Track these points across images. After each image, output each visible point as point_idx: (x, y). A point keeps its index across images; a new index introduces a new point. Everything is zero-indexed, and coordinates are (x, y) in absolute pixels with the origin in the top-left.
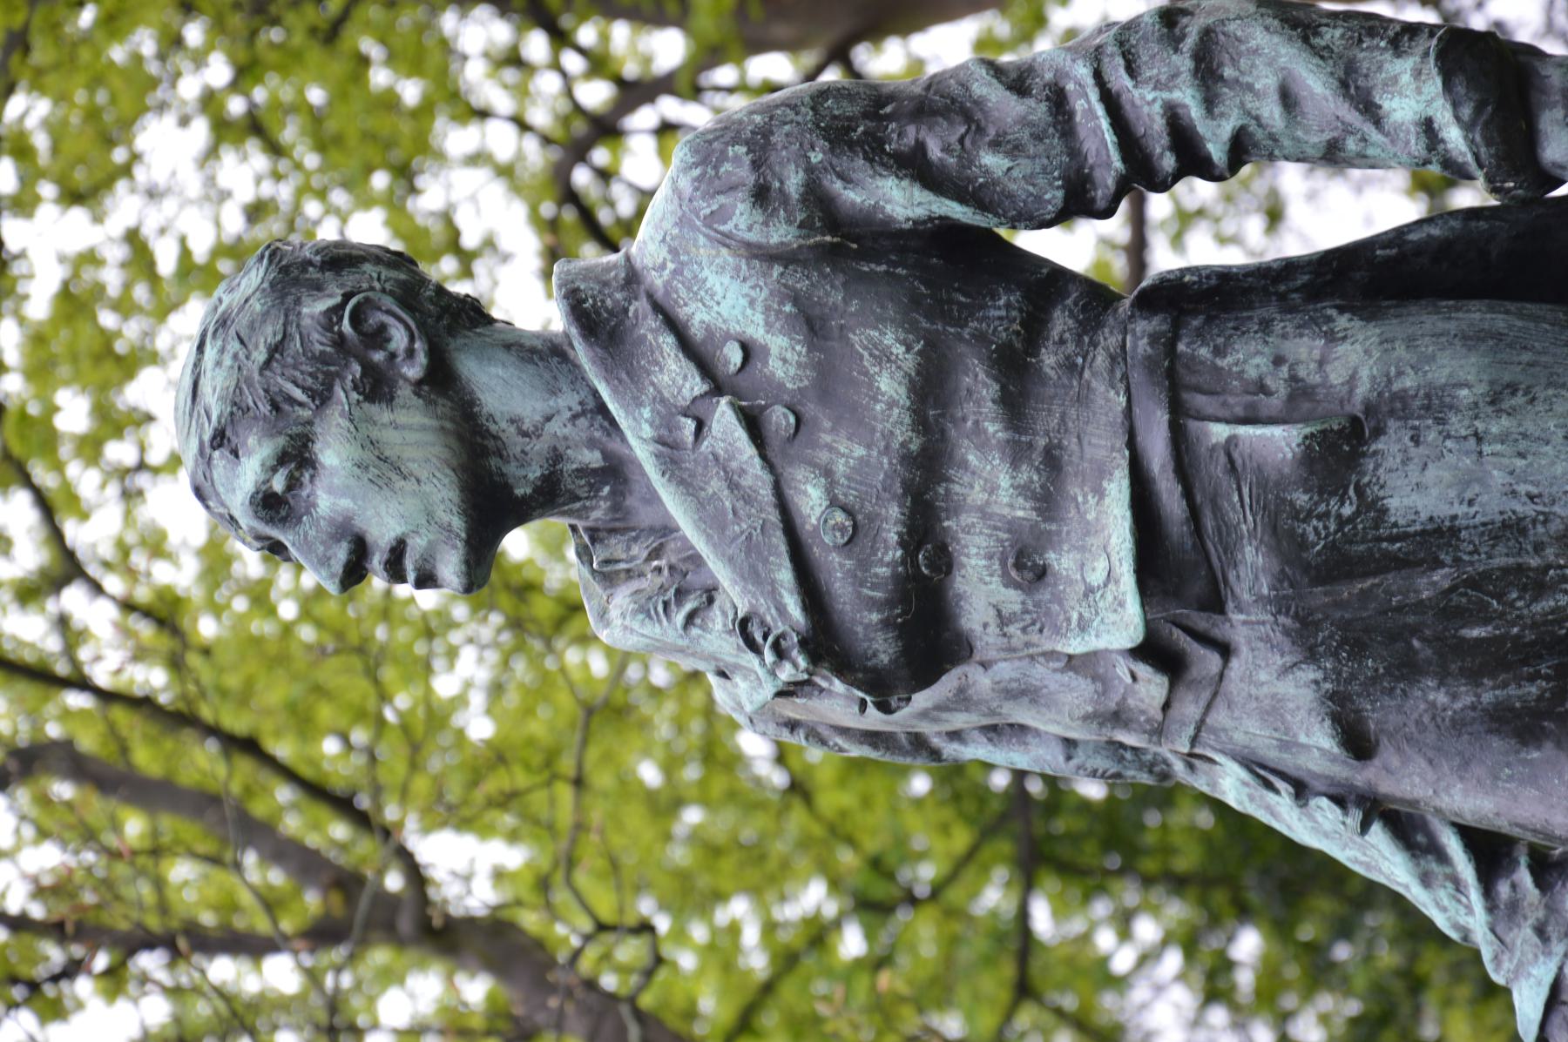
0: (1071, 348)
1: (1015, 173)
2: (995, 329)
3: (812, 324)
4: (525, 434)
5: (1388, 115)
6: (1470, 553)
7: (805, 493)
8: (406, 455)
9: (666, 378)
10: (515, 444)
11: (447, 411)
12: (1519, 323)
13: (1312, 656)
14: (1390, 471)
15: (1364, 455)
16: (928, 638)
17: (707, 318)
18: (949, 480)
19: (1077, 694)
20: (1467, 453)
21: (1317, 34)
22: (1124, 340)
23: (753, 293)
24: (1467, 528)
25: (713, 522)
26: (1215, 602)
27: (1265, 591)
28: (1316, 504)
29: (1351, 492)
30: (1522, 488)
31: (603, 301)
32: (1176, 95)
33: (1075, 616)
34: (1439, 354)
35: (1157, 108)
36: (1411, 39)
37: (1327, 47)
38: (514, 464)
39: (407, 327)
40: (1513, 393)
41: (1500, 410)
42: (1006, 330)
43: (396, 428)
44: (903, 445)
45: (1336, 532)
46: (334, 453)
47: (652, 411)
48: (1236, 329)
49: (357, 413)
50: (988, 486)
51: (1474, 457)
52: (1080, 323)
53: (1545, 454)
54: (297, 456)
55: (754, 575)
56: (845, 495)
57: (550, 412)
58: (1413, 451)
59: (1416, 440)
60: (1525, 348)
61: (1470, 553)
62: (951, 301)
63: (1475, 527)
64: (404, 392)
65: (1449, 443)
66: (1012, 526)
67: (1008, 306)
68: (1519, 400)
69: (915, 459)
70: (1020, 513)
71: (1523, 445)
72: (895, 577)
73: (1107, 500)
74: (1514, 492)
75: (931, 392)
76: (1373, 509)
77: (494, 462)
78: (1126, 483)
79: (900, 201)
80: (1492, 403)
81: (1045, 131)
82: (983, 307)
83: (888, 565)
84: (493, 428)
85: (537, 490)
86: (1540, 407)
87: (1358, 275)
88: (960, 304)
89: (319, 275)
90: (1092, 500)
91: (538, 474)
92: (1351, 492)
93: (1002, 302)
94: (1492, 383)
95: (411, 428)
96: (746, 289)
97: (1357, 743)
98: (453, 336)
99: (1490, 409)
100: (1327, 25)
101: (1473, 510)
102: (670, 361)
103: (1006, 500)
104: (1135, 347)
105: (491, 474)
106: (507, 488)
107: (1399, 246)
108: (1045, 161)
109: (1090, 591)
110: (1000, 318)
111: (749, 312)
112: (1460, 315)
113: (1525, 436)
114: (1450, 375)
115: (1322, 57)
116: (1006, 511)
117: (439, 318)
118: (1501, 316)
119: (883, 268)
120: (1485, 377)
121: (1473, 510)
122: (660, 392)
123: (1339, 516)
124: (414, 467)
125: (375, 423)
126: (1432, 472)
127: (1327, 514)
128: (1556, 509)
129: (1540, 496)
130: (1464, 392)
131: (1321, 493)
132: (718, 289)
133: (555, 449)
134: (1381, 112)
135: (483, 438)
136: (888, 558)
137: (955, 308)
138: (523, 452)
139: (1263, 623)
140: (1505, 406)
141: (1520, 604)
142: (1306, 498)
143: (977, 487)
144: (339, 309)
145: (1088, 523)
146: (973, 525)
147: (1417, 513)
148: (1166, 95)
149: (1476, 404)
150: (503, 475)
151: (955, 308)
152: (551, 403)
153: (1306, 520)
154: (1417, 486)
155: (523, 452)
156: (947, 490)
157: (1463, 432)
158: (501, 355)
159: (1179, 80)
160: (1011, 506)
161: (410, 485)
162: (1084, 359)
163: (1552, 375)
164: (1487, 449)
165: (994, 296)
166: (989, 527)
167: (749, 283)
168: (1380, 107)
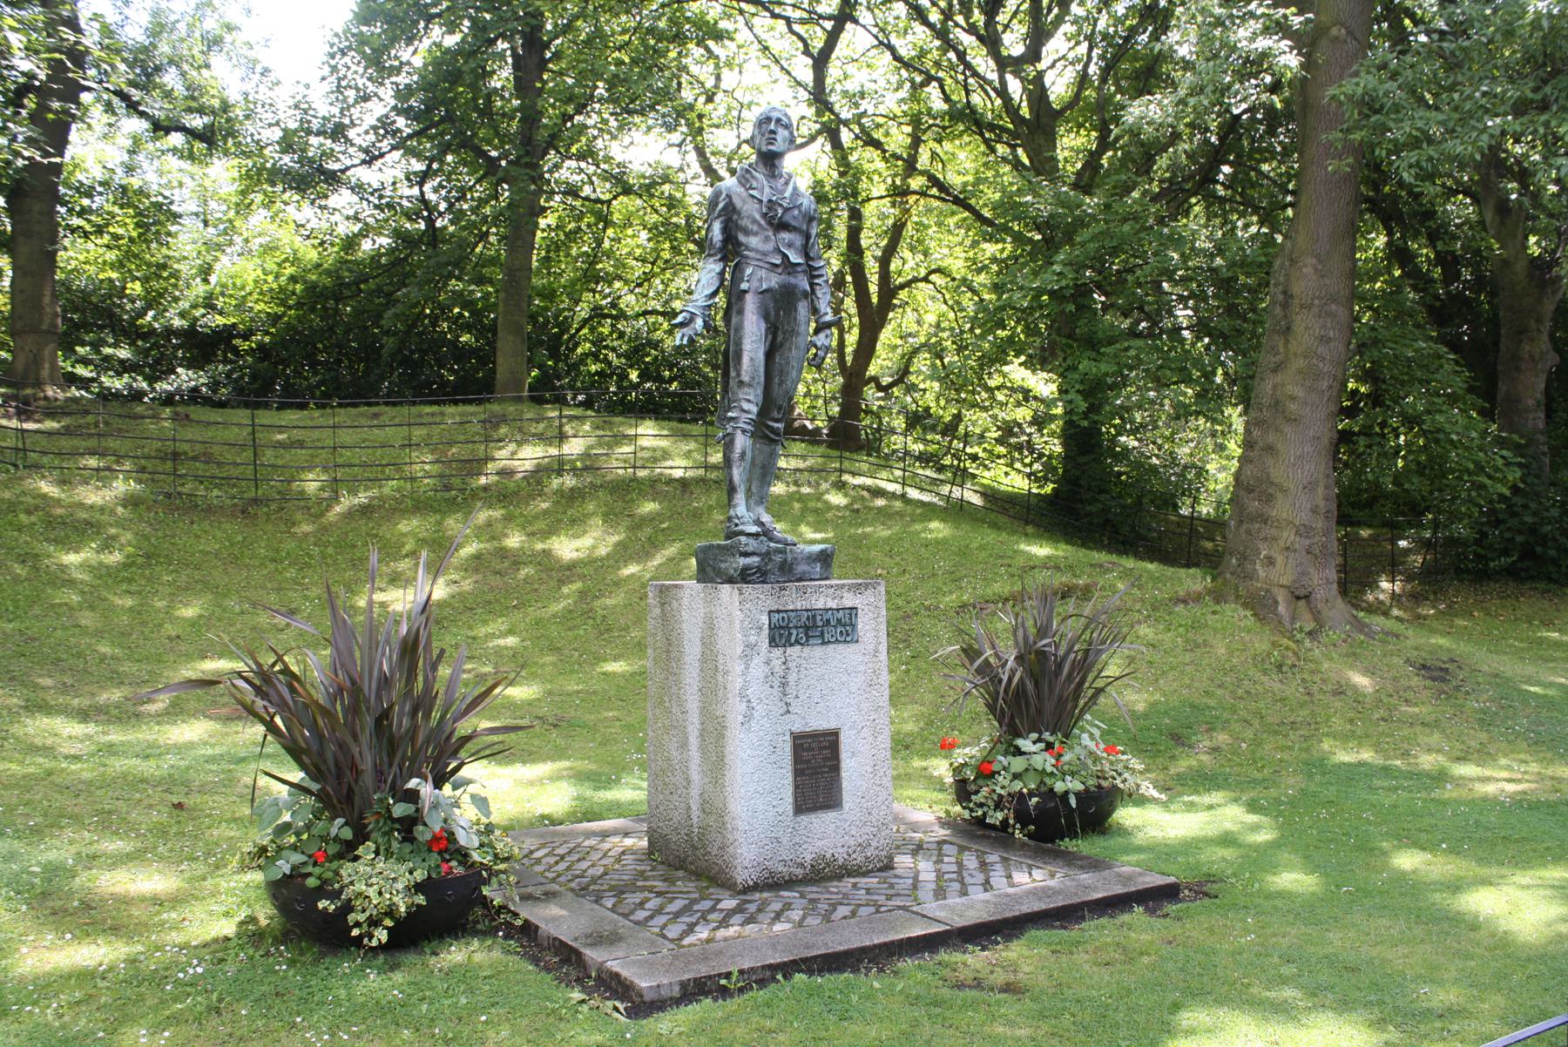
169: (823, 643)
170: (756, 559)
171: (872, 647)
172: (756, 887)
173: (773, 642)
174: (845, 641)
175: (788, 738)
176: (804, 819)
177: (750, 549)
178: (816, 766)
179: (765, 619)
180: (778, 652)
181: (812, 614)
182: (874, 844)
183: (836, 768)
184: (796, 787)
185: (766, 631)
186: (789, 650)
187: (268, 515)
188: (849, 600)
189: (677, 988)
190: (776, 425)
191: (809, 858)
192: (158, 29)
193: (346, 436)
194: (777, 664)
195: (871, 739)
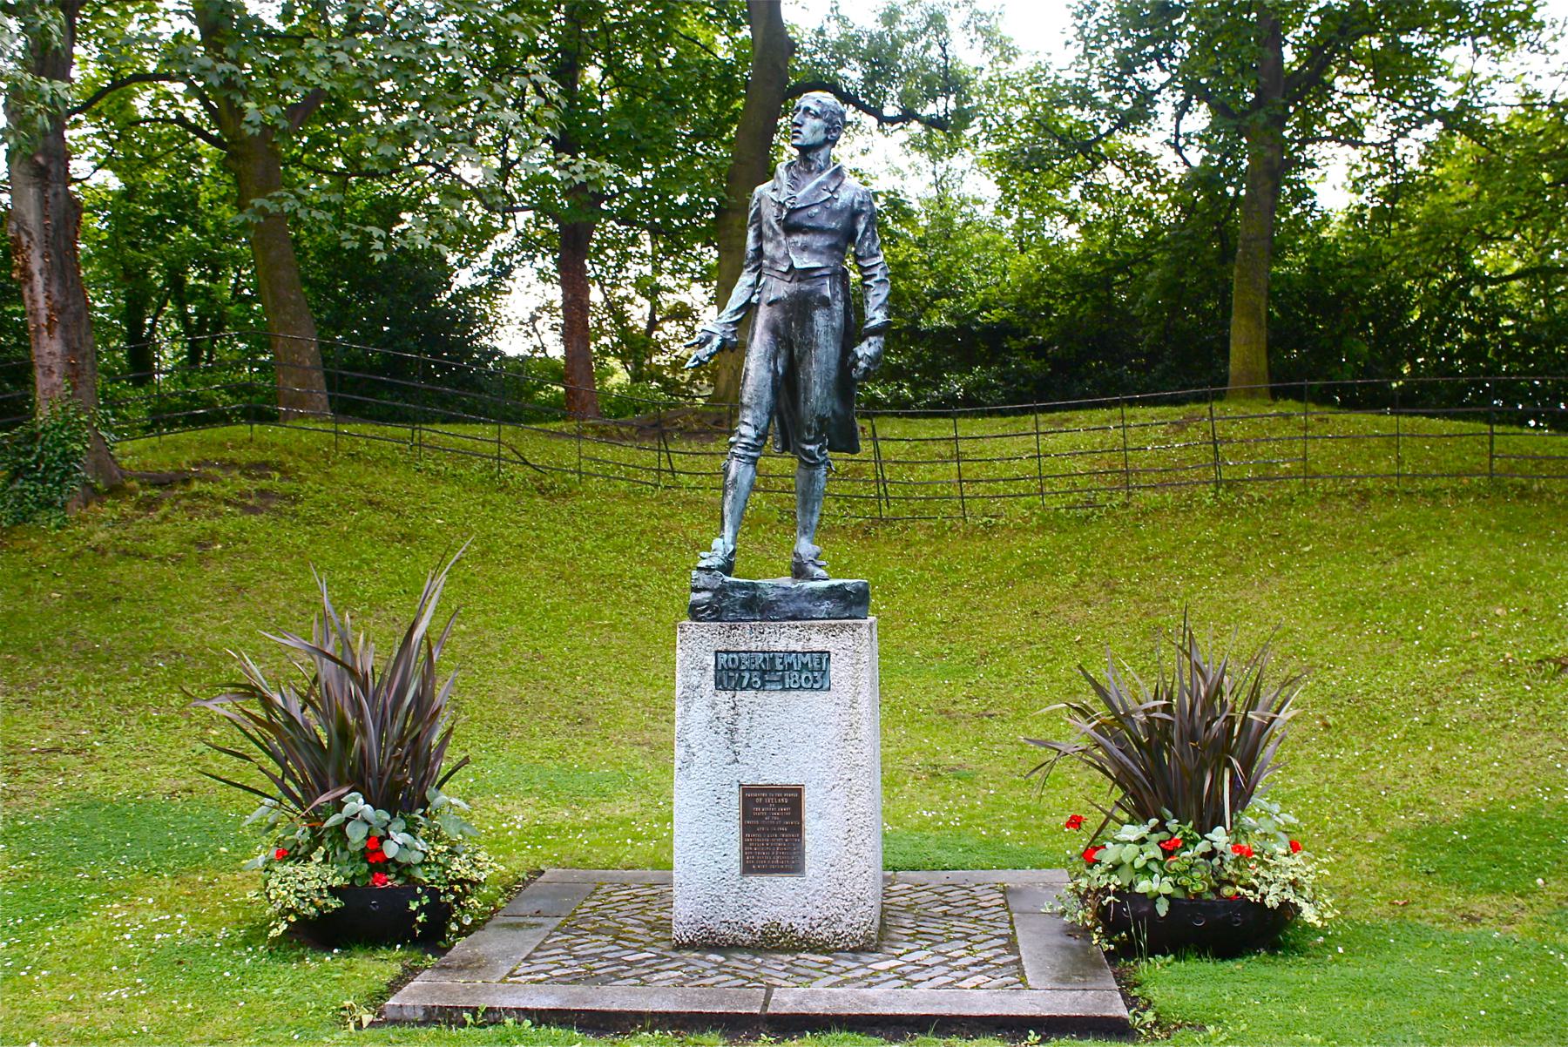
3: (842, 211)
16: (790, 228)
19: (780, 254)
25: (810, 192)
26: (799, 280)
46: (817, 122)
50: (820, 242)
54: (816, 116)
55: (805, 198)
75: (831, 232)
76: (816, 308)
79: (861, 227)
95: (821, 136)
97: (770, 304)
154: (820, 318)
169: (784, 689)
170: (708, 595)
171: (849, 696)
172: (691, 946)
173: (719, 684)
174: (812, 688)
175: (735, 789)
176: (754, 880)
177: (700, 584)
178: (772, 826)
179: (711, 660)
180: (725, 696)
181: (771, 657)
182: (847, 920)
183: (798, 829)
184: (745, 844)
185: (711, 672)
186: (739, 694)
187: (889, 535)
188: (818, 642)
189: (421, 1013)
190: (808, 447)
191: (759, 924)
192: (890, 17)
193: (1049, 441)
194: (724, 709)
195: (845, 801)
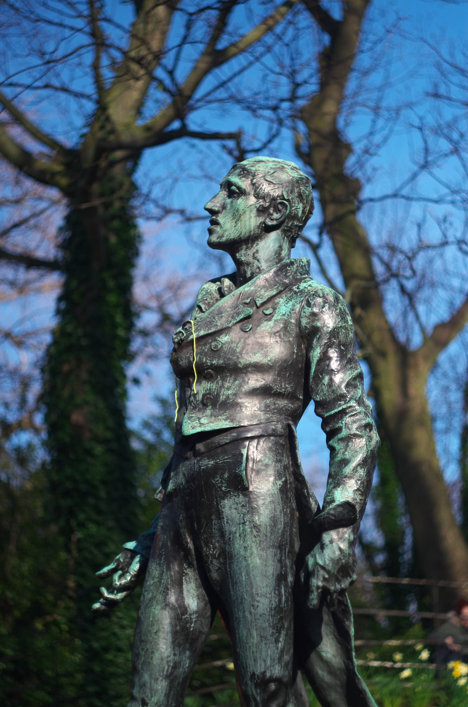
0: (273, 407)
1: (323, 386)
2: (277, 385)
4: (254, 254)
5: (336, 490)
6: (215, 523)
7: (226, 336)
8: (242, 222)
9: (262, 293)
10: (251, 252)
11: (257, 232)
12: (280, 531)
13: (187, 482)
14: (234, 500)
15: (238, 492)
17: (281, 302)
18: (231, 376)
20: (240, 520)
21: (361, 468)
22: (275, 422)
23: (286, 315)
24: (221, 522)
27: (202, 468)
28: (225, 480)
29: (228, 489)
30: (231, 536)
31: (289, 272)
32: (344, 430)
33: (193, 415)
34: (268, 510)
35: (340, 425)
36: (359, 494)
37: (357, 471)
38: (245, 252)
39: (280, 218)
40: (257, 532)
41: (252, 528)
42: (277, 388)
43: (250, 218)
44: (240, 362)
45: (218, 486)
47: (253, 290)
48: (278, 453)
49: (253, 207)
51: (239, 522)
52: (282, 408)
53: (240, 542)
56: (225, 347)
57: (260, 261)
58: (240, 505)
59: (243, 506)
60: (271, 534)
61: (215, 523)
62: (286, 371)
63: (221, 524)
64: (261, 220)
65: (242, 515)
66: (218, 395)
67: (286, 388)
68: (255, 533)
69: (236, 366)
70: (221, 397)
71: (243, 535)
72: (203, 363)
73: (223, 421)
74: (230, 534)
76: (225, 495)
77: (244, 247)
78: (228, 426)
80: (254, 526)
81: (335, 393)
82: (285, 381)
83: (206, 361)
84: (254, 245)
85: (238, 259)
86: (254, 539)
87: (299, 485)
88: (286, 374)
89: (296, 191)
90: (224, 417)
91: (243, 259)
92: (228, 489)
93: (287, 386)
94: (260, 525)
96: (288, 313)
98: (281, 231)
99: (252, 525)
100: (364, 470)
101: (225, 523)
102: (267, 294)
103: (225, 393)
104: (272, 425)
105: (241, 246)
106: (238, 251)
107: (308, 496)
108: (327, 394)
109: (199, 419)
110: (281, 386)
111: (281, 314)
112: (282, 515)
113: (245, 536)
114: (261, 514)
115: (353, 470)
116: (222, 393)
117: (287, 226)
118: (283, 526)
119: (296, 351)
120: (261, 523)
121: (225, 523)
122: (259, 291)
123: (222, 486)
124: (239, 224)
125: (250, 212)
126: (234, 511)
127: (222, 483)
128: (227, 546)
129: (230, 541)
130: (257, 518)
131: (227, 481)
132: (289, 304)
133: (250, 263)
134: (337, 488)
135: (251, 243)
136: (208, 361)
137: (284, 373)
138: (249, 254)
139: (194, 468)
140: (253, 530)
141: (203, 538)
142: (226, 477)
143: (228, 384)
144: (284, 199)
145: (218, 417)
146: (218, 384)
147: (224, 508)
148: (344, 427)
149: (253, 522)
150: (241, 250)
151: (284, 373)
152: (263, 261)
153: (220, 478)
155: (249, 254)
156: (228, 376)
157: (245, 519)
158: (277, 245)
159: (348, 430)
160: (223, 394)
161: (234, 224)
162: (269, 411)
163: (263, 542)
164: (241, 526)
165: (289, 384)
166: (218, 389)
167: (289, 313)
168: (339, 487)
